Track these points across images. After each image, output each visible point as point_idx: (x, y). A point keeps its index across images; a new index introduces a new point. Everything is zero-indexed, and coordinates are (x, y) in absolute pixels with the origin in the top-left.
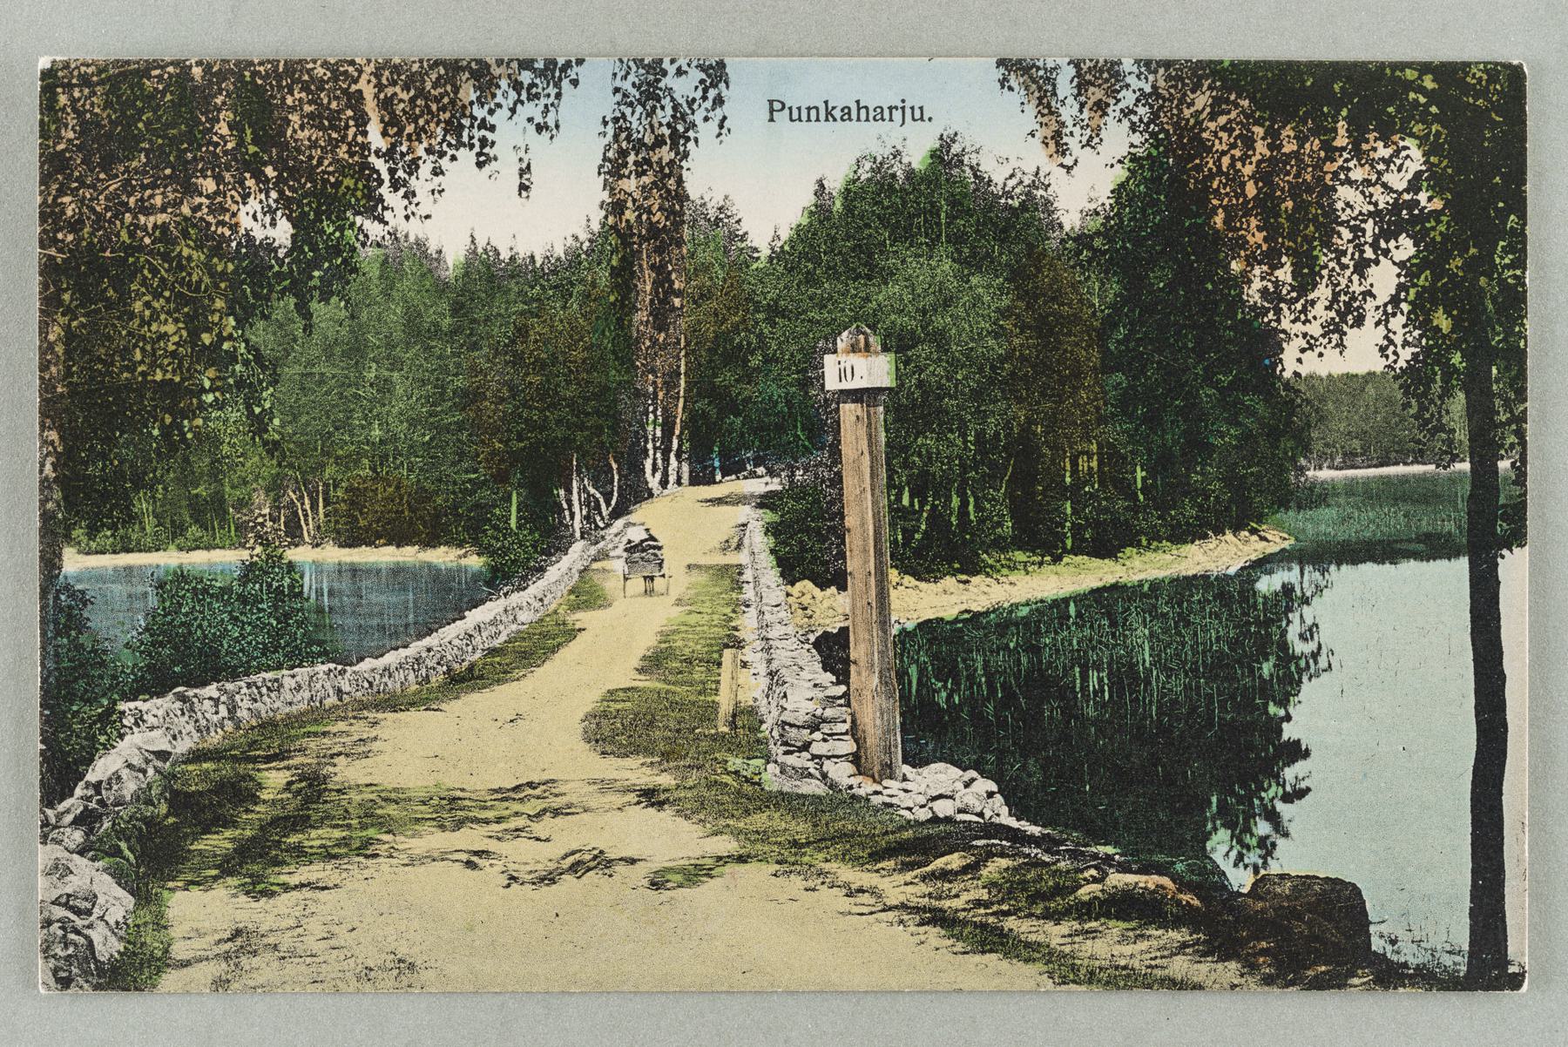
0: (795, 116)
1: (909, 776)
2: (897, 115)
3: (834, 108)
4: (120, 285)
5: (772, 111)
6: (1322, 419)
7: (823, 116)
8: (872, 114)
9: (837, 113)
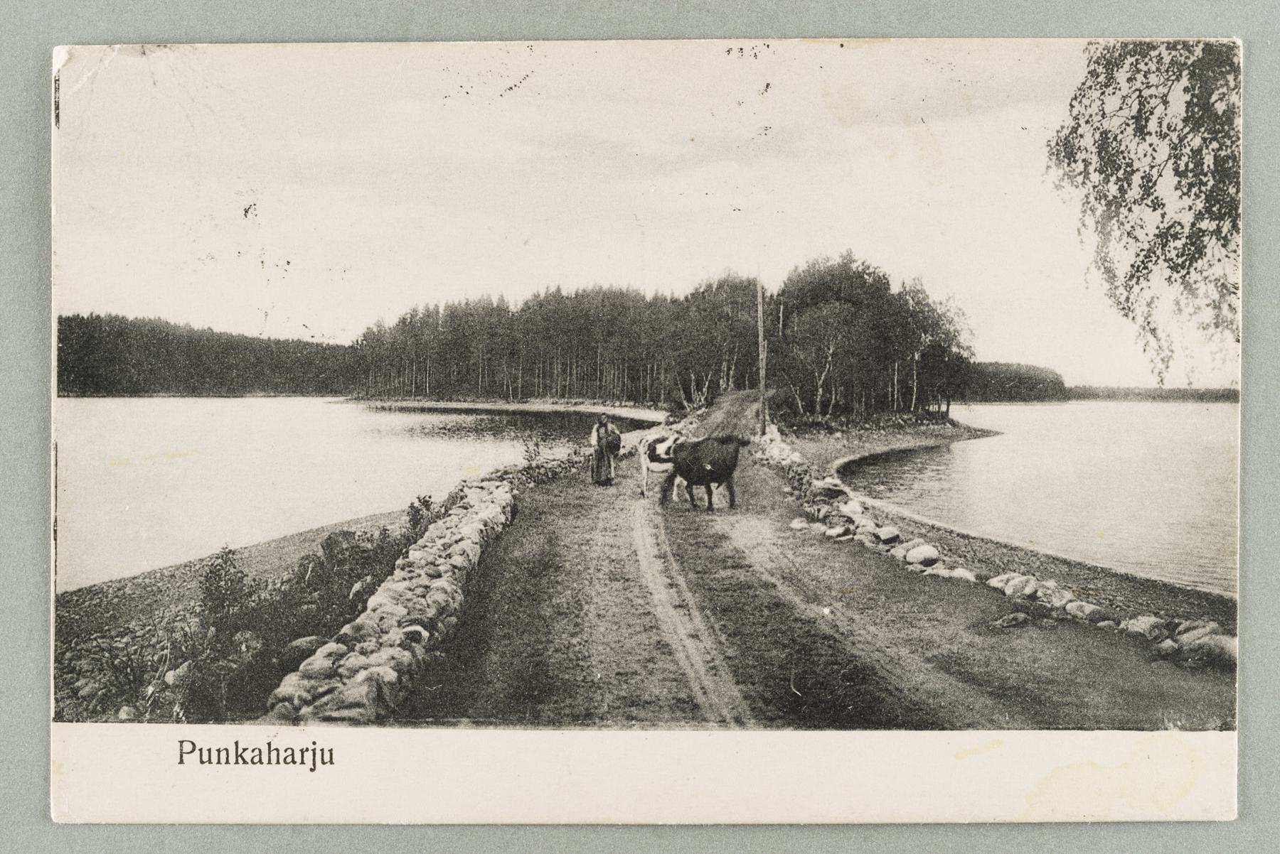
0: (205, 758)
2: (309, 756)
3: (245, 750)
7: (232, 758)
9: (248, 756)
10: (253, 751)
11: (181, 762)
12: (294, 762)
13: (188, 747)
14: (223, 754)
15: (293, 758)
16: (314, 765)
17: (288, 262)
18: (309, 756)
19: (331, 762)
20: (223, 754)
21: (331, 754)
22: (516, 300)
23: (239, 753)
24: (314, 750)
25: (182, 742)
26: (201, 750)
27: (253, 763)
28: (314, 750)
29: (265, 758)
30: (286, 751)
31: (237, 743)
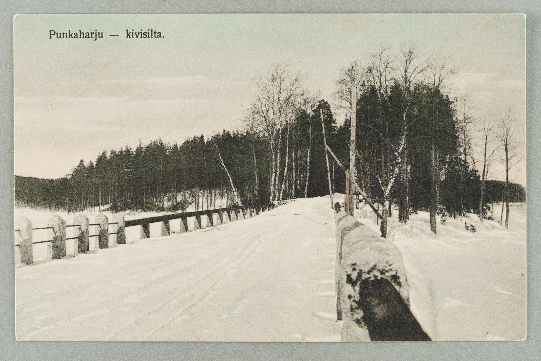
0: (59, 36)
2: (94, 35)
3: (72, 34)
5: (51, 34)
7: (68, 36)
8: (85, 35)
9: (73, 35)
10: (75, 34)
11: (51, 38)
12: (77, 37)
13: (53, 33)
14: (65, 35)
15: (77, 36)
18: (94, 35)
19: (102, 37)
20: (65, 35)
21: (102, 34)
25: (50, 31)
26: (57, 33)
27: (158, 37)
28: (133, 33)
29: (79, 36)
31: (69, 31)
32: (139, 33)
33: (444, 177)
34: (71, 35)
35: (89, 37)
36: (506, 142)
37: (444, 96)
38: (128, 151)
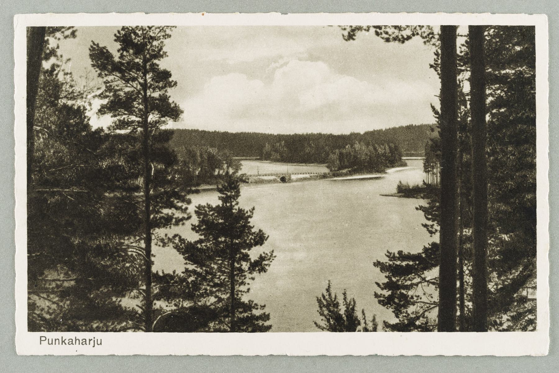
0: (50, 342)
1: (250, 283)
2: (92, 342)
4: (383, 154)
5: (41, 340)
6: (295, 242)
8: (81, 342)
9: (67, 342)
11: (41, 344)
12: (72, 344)
16: (94, 344)
17: (401, 336)
18: (92, 342)
19: (101, 344)
22: (276, 134)
23: (63, 340)
24: (94, 341)
26: (49, 339)
29: (74, 342)
30: (82, 340)
31: (62, 337)
32: (90, 340)
33: (176, 168)
34: (64, 342)
35: (73, 343)
36: (131, 86)
37: (342, 315)
38: (412, 125)
